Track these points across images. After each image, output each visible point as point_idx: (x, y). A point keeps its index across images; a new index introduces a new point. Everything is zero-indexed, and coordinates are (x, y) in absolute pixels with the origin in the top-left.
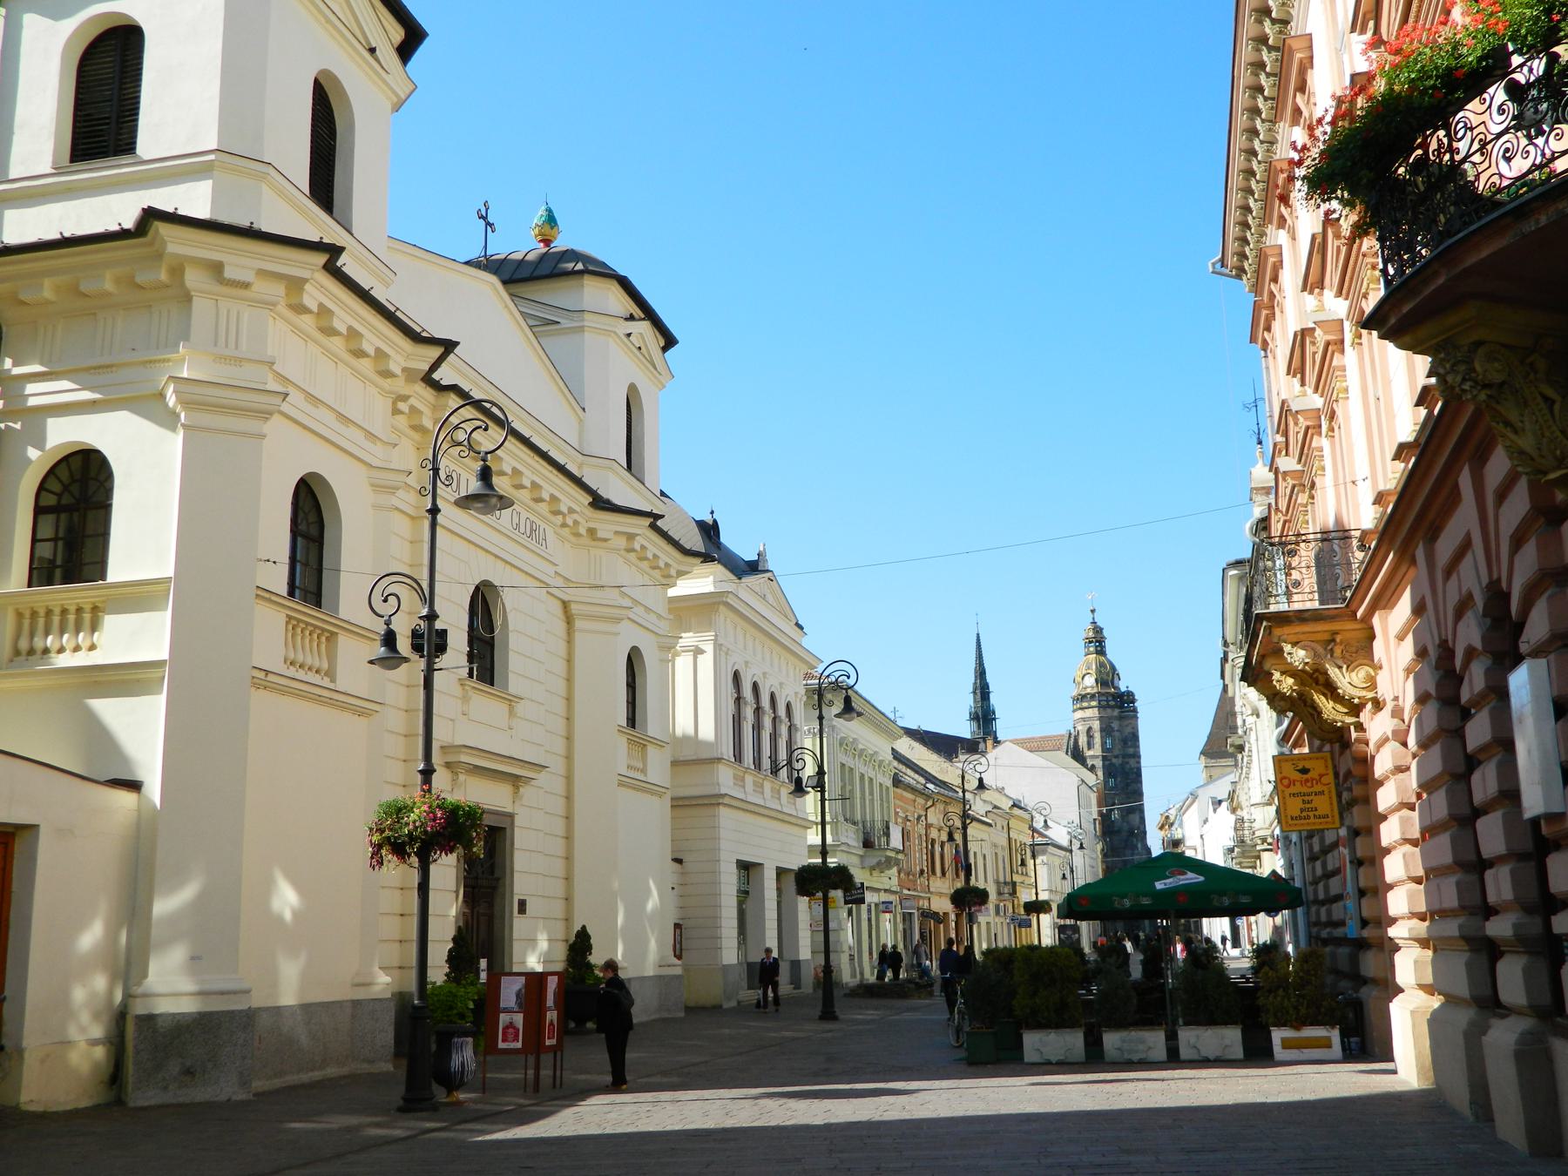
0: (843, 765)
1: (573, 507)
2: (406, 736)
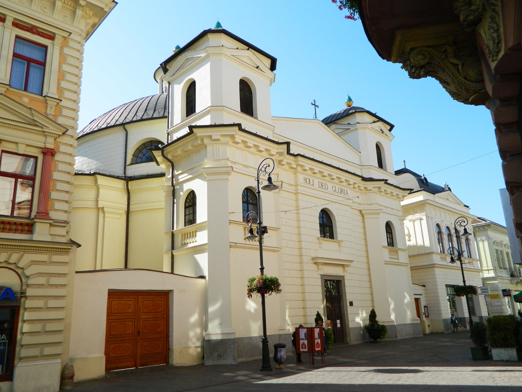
0: (497, 250)
1: (355, 182)
2: (300, 256)
